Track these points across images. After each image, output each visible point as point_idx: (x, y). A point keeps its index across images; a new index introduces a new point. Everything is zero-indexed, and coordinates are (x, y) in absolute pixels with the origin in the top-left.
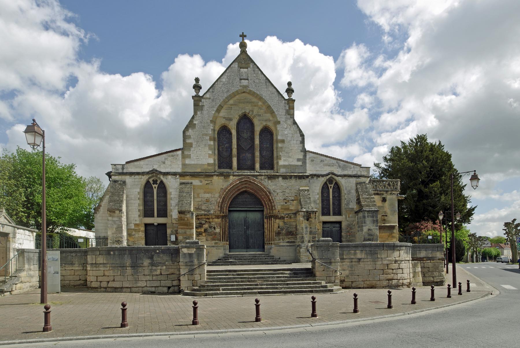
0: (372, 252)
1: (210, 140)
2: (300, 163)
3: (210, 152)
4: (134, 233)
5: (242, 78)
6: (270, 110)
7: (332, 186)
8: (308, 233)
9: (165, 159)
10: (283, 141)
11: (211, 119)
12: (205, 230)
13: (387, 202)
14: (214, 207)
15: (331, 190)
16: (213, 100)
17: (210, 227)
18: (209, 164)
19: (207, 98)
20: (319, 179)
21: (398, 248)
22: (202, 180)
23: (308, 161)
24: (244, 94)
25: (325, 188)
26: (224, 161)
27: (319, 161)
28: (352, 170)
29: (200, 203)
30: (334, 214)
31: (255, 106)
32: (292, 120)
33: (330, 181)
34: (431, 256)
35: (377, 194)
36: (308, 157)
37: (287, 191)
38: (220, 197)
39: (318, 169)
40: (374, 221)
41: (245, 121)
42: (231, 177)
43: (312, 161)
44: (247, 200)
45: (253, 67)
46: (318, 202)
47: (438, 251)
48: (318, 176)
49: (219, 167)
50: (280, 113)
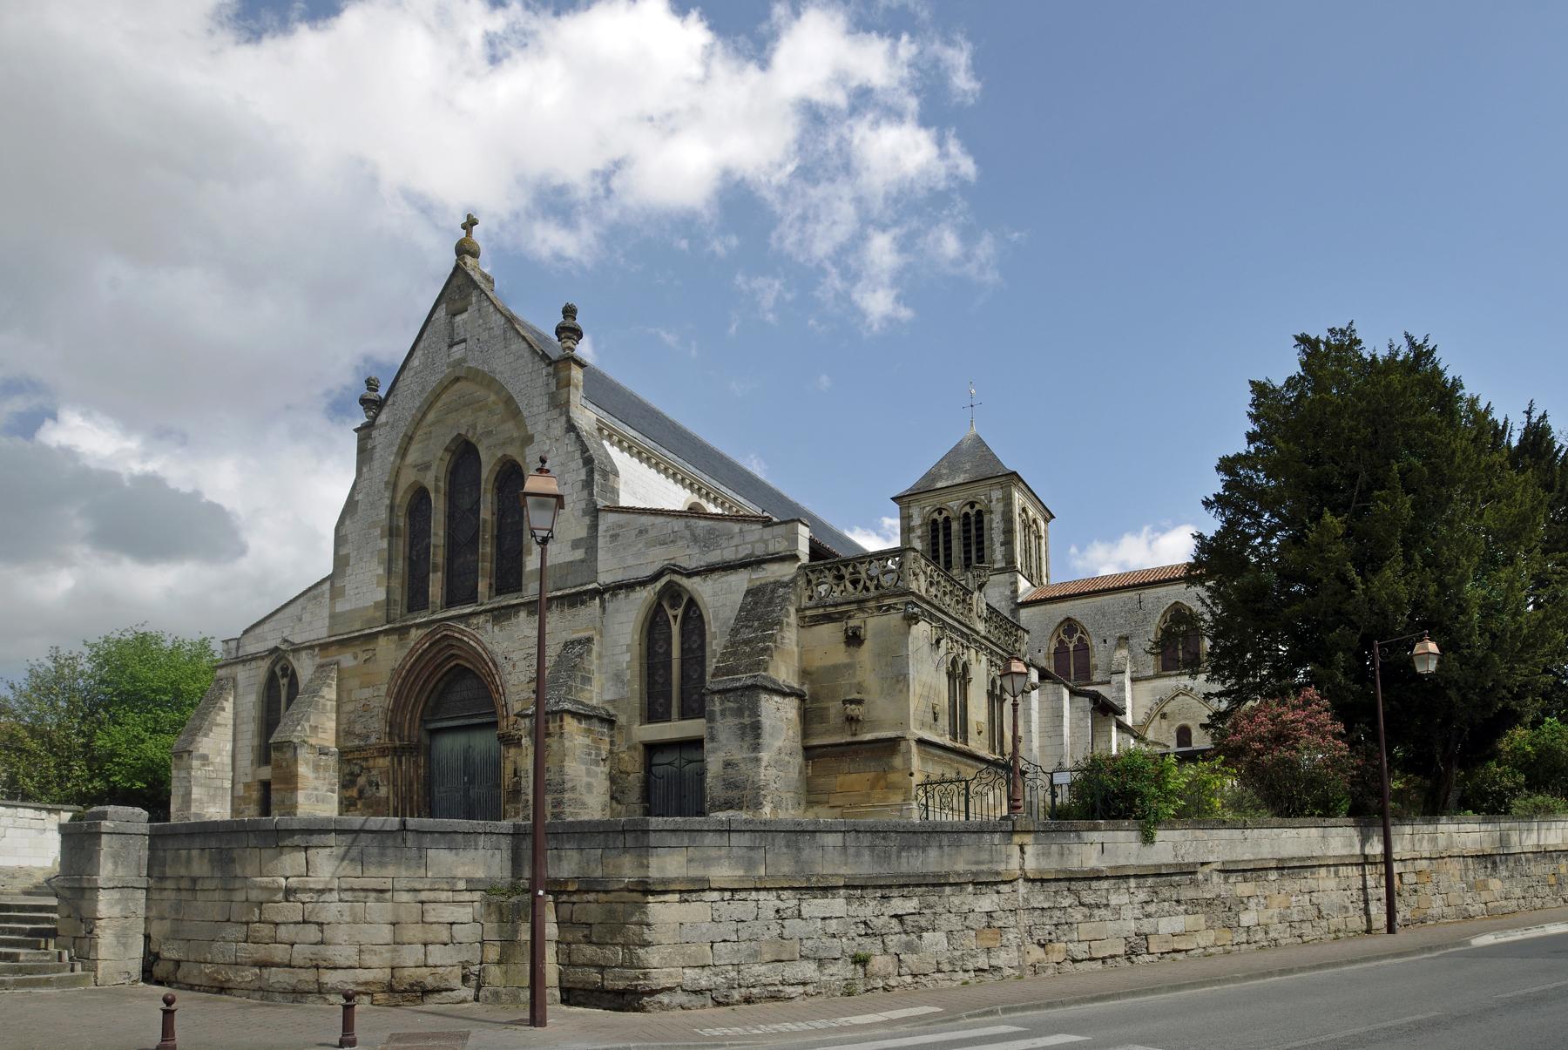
3: (381, 571)
6: (513, 411)
7: (680, 612)
12: (361, 792)
15: (676, 629)
17: (370, 783)
18: (377, 605)
20: (633, 595)
21: (297, 839)
22: (357, 650)
24: (458, 386)
25: (654, 625)
27: (634, 533)
28: (735, 541)
32: (564, 419)
34: (598, 873)
35: (828, 618)
38: (388, 694)
39: (630, 561)
40: (743, 727)
41: (464, 454)
42: (413, 631)
43: (614, 537)
44: (447, 689)
45: (479, 301)
46: (628, 675)
47: (626, 849)
48: (629, 586)
50: (535, 410)
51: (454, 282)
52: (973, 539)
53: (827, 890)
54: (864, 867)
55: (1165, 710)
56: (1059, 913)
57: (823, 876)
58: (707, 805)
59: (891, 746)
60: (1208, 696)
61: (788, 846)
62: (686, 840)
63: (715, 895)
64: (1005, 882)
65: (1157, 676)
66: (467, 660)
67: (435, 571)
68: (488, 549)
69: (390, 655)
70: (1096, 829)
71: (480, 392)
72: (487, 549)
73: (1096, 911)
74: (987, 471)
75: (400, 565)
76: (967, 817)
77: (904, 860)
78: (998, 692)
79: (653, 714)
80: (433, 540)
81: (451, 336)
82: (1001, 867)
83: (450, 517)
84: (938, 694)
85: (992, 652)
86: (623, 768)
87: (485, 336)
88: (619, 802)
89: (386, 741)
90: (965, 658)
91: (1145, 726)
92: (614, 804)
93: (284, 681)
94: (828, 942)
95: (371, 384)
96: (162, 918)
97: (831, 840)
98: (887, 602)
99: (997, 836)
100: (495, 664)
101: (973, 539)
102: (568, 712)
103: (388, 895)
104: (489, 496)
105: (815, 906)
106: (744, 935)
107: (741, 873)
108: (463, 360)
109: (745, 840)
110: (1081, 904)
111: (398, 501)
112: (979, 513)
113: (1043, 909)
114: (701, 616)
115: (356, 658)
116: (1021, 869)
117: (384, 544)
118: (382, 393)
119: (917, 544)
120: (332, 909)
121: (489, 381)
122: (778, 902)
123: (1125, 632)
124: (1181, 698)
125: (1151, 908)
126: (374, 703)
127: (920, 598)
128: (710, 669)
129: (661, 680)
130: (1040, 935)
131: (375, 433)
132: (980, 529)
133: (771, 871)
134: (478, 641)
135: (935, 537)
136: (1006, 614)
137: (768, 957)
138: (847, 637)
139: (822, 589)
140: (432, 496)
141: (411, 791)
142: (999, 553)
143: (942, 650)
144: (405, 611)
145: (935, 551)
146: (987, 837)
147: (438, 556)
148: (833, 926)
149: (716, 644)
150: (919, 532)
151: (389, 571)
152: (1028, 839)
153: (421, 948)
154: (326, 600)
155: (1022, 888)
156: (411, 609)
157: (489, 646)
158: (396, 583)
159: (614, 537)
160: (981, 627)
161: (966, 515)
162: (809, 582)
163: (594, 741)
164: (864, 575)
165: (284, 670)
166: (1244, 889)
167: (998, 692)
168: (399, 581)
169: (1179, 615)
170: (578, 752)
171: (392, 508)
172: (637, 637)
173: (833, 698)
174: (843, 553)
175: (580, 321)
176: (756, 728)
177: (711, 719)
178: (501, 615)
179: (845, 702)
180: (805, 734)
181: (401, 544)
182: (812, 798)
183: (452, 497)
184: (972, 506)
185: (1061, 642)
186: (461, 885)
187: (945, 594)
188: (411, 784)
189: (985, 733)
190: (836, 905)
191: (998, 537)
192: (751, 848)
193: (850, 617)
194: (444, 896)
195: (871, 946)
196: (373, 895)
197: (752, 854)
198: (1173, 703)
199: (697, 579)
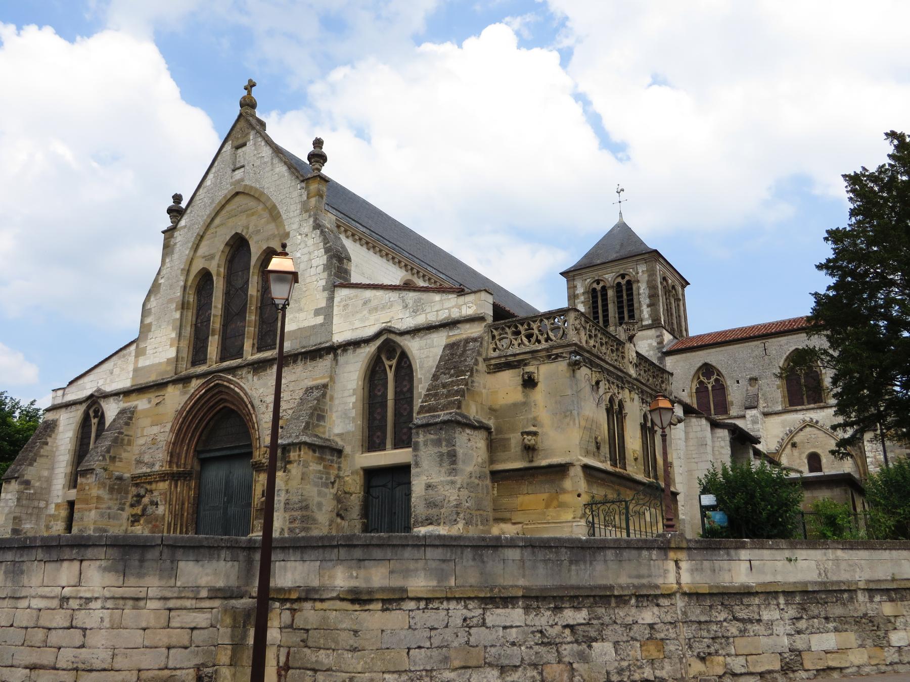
1: (176, 310)
3: (173, 335)
6: (274, 214)
7: (394, 362)
11: (182, 267)
12: (144, 510)
13: (540, 386)
15: (391, 375)
20: (359, 351)
23: (336, 310)
25: (374, 375)
30: (396, 446)
31: (253, 214)
34: (315, 583)
35: (508, 366)
39: (358, 324)
40: (441, 455)
41: (238, 245)
43: (346, 306)
45: (255, 138)
48: (356, 344)
50: (292, 214)
51: (238, 126)
52: (625, 302)
53: (507, 601)
54: (540, 577)
55: (796, 439)
56: (714, 627)
57: (504, 588)
58: (412, 520)
59: (561, 470)
60: (834, 428)
61: (474, 559)
62: (389, 553)
63: (412, 605)
64: (663, 596)
65: (785, 412)
66: (234, 404)
67: (213, 335)
68: (253, 318)
69: (175, 399)
70: (743, 546)
71: (252, 203)
72: (252, 317)
73: (749, 626)
74: (632, 249)
75: (188, 331)
76: (628, 535)
77: (573, 573)
78: (649, 424)
79: (373, 443)
80: (213, 312)
81: (234, 163)
82: (660, 581)
83: (227, 294)
84: (598, 427)
85: (642, 392)
86: (347, 490)
87: (257, 163)
88: (342, 518)
89: (166, 468)
90: (620, 397)
91: (778, 452)
92: (339, 520)
93: (95, 421)
94: (510, 650)
95: (177, 198)
97: (513, 554)
98: (555, 351)
99: (655, 552)
100: (253, 406)
101: (625, 302)
102: (305, 443)
103: (142, 603)
104: (256, 278)
105: (497, 616)
106: (436, 642)
107: (434, 583)
108: (242, 180)
109: (438, 553)
110: (735, 619)
113: (700, 623)
114: (410, 366)
115: (150, 402)
116: (678, 583)
117: (177, 315)
118: (183, 205)
119: (581, 308)
120: (93, 617)
122: (465, 611)
123: (754, 374)
124: (808, 429)
125: (802, 624)
127: (581, 348)
128: (416, 408)
129: (378, 417)
130: (700, 647)
131: (176, 234)
133: (460, 582)
134: (241, 388)
135: (595, 302)
136: (656, 361)
137: (457, 663)
138: (524, 381)
139: (505, 343)
140: (215, 278)
141: (182, 509)
142: (646, 312)
143: (601, 391)
144: (189, 365)
145: (596, 313)
146: (645, 553)
147: (216, 323)
148: (513, 634)
149: (421, 387)
150: (582, 298)
151: (180, 335)
152: (682, 555)
153: (164, 650)
154: (132, 358)
155: (680, 602)
156: (194, 364)
157: (248, 391)
158: (184, 344)
159: (346, 306)
160: (632, 372)
162: (493, 337)
163: (325, 467)
164: (536, 331)
165: (96, 412)
166: (888, 609)
167: (649, 424)
168: (187, 342)
169: (801, 360)
170: (312, 477)
171: (185, 287)
172: (360, 383)
174: (522, 314)
175: (325, 149)
176: (452, 456)
177: (416, 449)
178: (258, 367)
179: (523, 433)
180: (492, 461)
181: (190, 315)
182: (499, 515)
185: (701, 383)
186: (204, 593)
187: (602, 344)
188: (183, 504)
189: (641, 460)
190: (516, 615)
191: (645, 301)
192: (444, 561)
193: (526, 365)
194: (188, 603)
195: (549, 655)
196: (130, 603)
197: (444, 566)
198: (802, 433)
199: (408, 337)
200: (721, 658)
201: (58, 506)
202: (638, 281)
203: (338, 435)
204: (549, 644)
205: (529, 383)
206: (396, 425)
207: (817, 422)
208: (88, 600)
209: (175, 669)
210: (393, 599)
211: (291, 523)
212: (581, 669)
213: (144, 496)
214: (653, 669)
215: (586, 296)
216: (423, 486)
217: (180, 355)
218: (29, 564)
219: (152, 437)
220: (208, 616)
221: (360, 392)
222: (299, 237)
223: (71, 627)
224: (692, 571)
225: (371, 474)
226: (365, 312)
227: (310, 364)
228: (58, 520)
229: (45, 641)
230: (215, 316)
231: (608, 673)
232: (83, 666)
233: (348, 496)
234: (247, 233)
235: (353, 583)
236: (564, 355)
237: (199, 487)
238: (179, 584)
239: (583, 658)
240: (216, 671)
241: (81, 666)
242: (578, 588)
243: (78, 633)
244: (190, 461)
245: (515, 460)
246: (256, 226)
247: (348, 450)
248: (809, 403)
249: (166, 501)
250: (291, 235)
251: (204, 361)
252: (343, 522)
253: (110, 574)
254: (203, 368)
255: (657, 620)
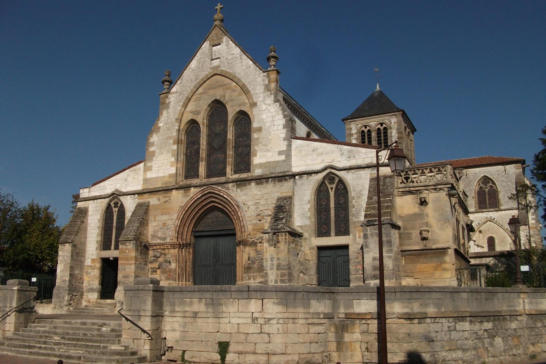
0: (215, 301)
1: (174, 144)
2: (283, 157)
3: (173, 159)
4: (90, 270)
5: (214, 57)
6: (245, 90)
7: (334, 186)
8: (275, 267)
9: (128, 175)
10: (260, 129)
11: (176, 117)
14: (170, 233)
15: (332, 194)
16: (180, 94)
17: (166, 261)
18: (170, 176)
19: (174, 93)
20: (310, 178)
23: (293, 153)
25: (321, 192)
26: (190, 169)
29: (157, 228)
30: (337, 234)
31: (228, 89)
33: (331, 177)
35: (410, 192)
36: (293, 146)
37: (262, 202)
39: (309, 162)
41: (218, 108)
48: (309, 173)
49: (186, 178)
50: (257, 92)
52: (382, 140)
56: (537, 330)
59: (443, 251)
67: (202, 161)
68: (231, 152)
69: (179, 200)
75: (182, 157)
82: (517, 309)
87: (230, 57)
96: (174, 330)
100: (238, 206)
109: (438, 295)
111: (182, 128)
112: (385, 128)
115: (159, 200)
117: (175, 147)
120: (273, 328)
121: (231, 78)
124: (489, 223)
126: (169, 222)
129: (324, 217)
132: (386, 135)
134: (229, 195)
137: (447, 348)
140: (201, 126)
148: (466, 334)
150: (355, 136)
158: (180, 165)
159: (300, 151)
161: (379, 129)
165: (116, 204)
171: (179, 130)
172: (313, 197)
173: (414, 229)
181: (183, 148)
183: (210, 126)
184: (382, 125)
186: (322, 316)
190: (466, 325)
196: (291, 321)
198: (485, 225)
200: (539, 344)
201: (93, 260)
202: (391, 128)
203: (299, 226)
204: (480, 338)
205: (423, 203)
206: (336, 222)
207: (494, 219)
208: (270, 319)
209: (314, 353)
210: (422, 318)
211: (282, 276)
212: (491, 350)
213: (159, 257)
214: (517, 350)
215: (358, 134)
216: (371, 259)
217: (178, 172)
218: (226, 300)
219: (163, 222)
220: (323, 327)
221: (313, 203)
222: (264, 106)
223: (261, 333)
224: (531, 303)
225: (320, 249)
226: (314, 155)
227: (278, 185)
228: (94, 269)
229: (246, 340)
230: (202, 149)
231: (501, 352)
232: (272, 352)
233: (307, 261)
234: (224, 100)
235: (407, 310)
236: (445, 189)
237: (194, 252)
238: (311, 311)
239: (492, 345)
240: (329, 354)
241: (270, 352)
242: (489, 312)
243: (266, 336)
244: (189, 237)
245: (415, 245)
246: (231, 96)
247: (306, 235)
248: (490, 208)
249: (176, 261)
250: (258, 104)
251: (197, 176)
252: (305, 277)
253: (280, 306)
254: (195, 181)
255: (517, 327)
